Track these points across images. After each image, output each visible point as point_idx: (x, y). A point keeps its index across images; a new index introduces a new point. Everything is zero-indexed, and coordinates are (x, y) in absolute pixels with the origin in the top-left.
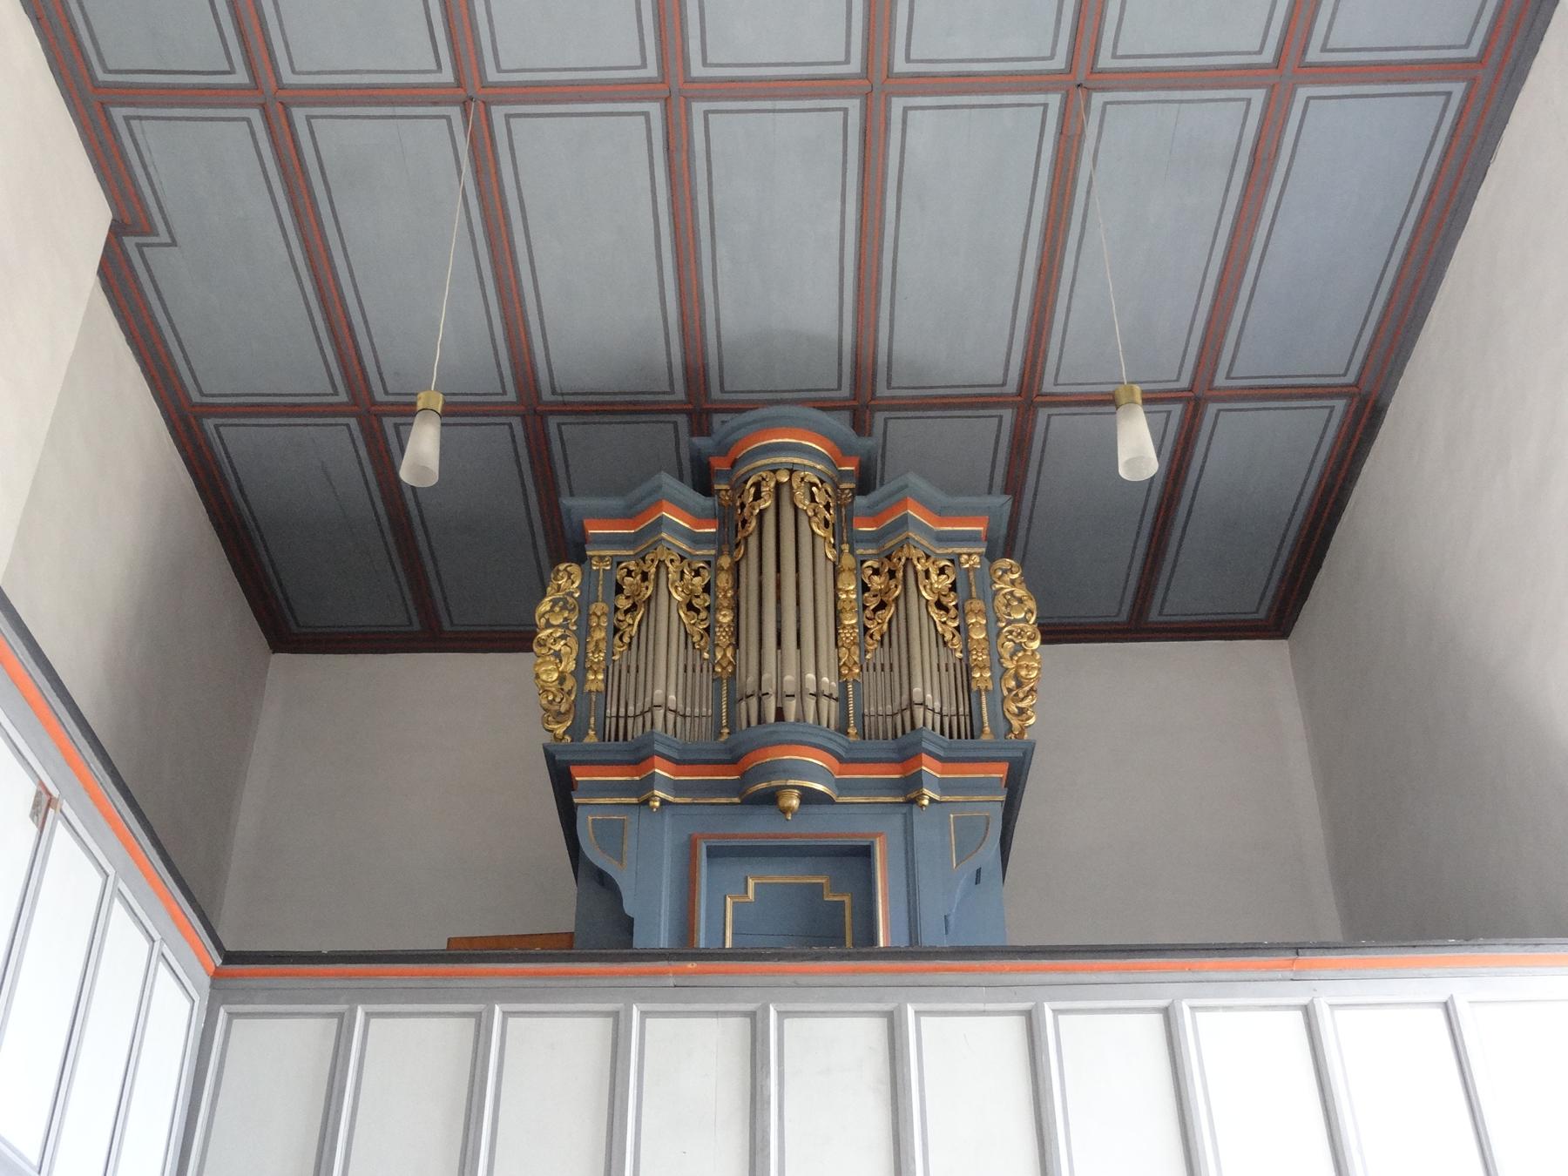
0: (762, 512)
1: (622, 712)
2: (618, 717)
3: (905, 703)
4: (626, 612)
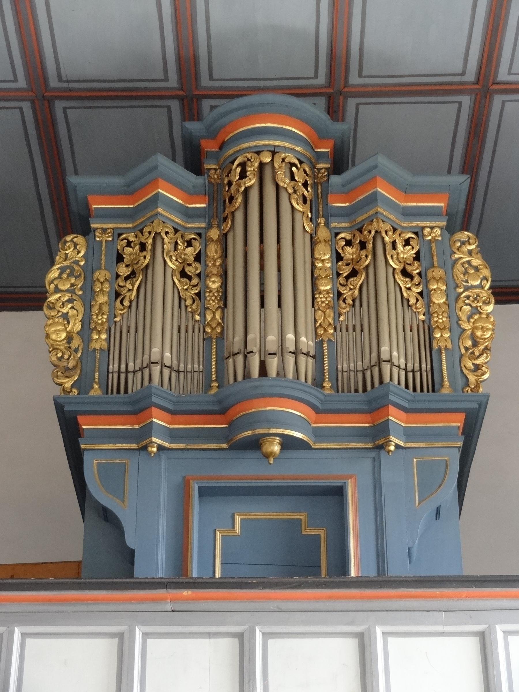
0: (247, 190)
2: (119, 372)
4: (126, 279)
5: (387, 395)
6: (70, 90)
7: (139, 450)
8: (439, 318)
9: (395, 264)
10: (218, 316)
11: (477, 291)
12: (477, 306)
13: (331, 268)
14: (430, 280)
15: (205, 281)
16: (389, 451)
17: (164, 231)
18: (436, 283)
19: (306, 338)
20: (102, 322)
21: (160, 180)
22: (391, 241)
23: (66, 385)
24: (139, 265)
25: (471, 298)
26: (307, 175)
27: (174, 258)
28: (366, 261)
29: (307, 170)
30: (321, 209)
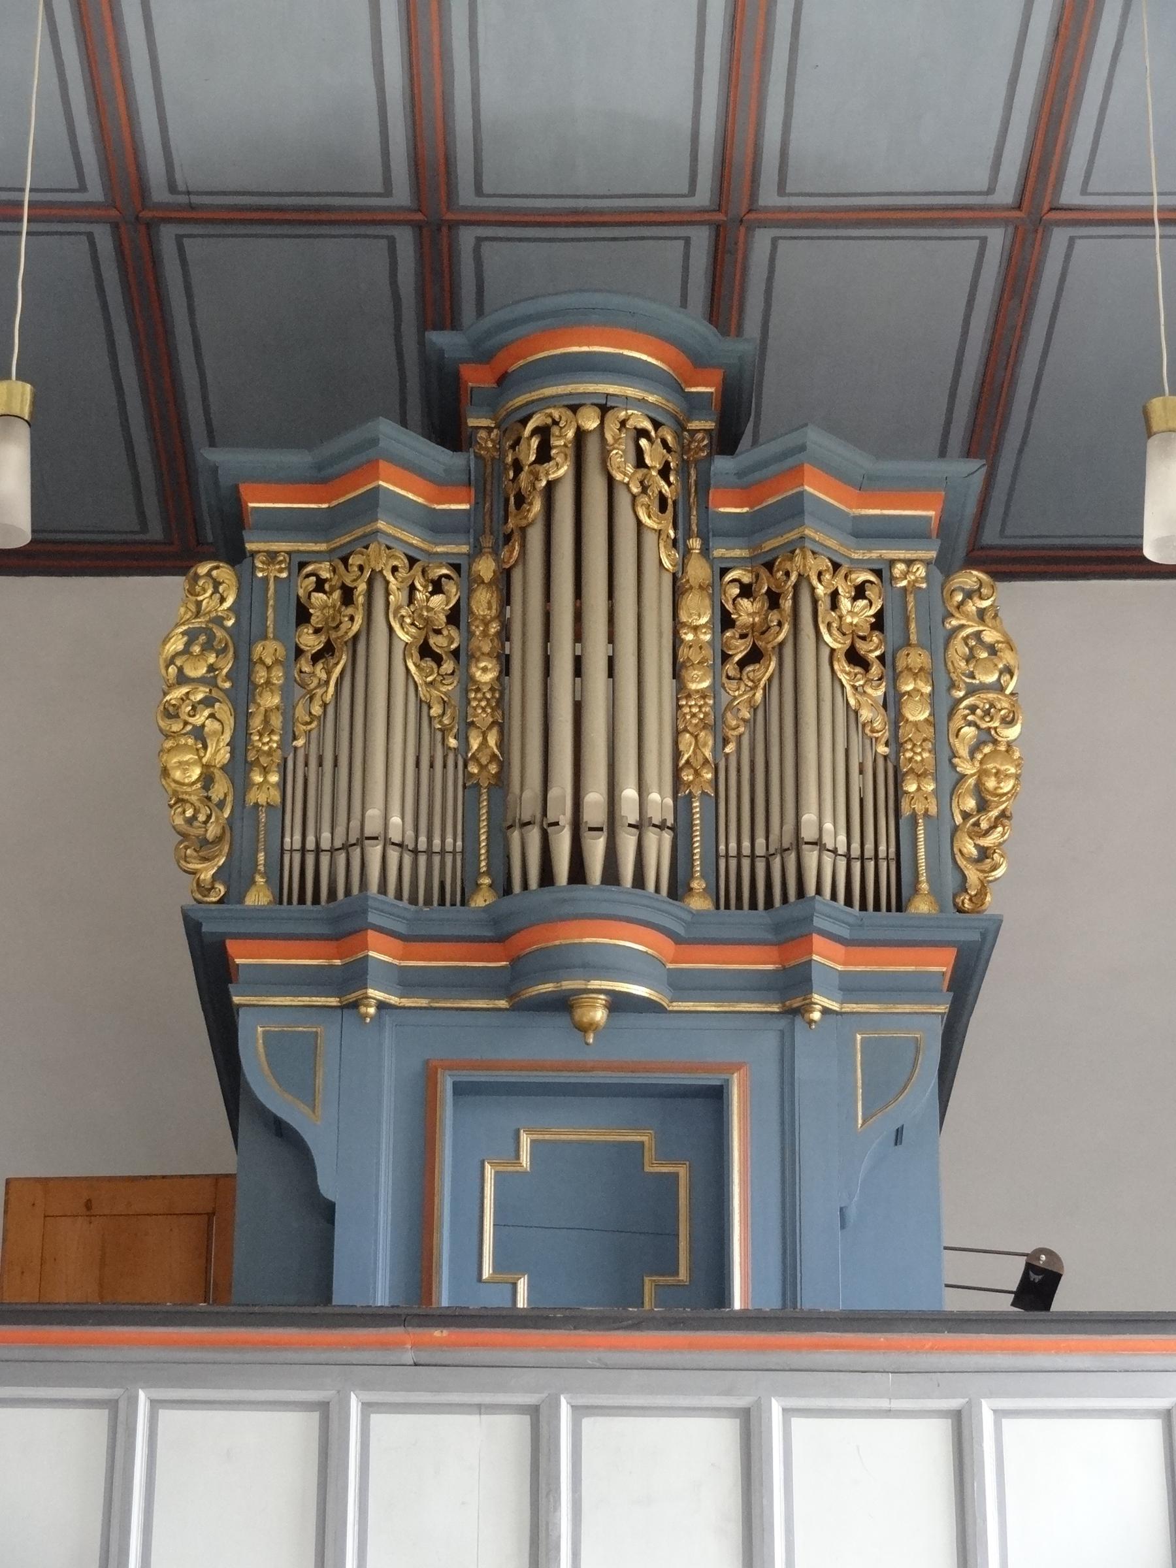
0: (551, 485)
1: (311, 843)
2: (303, 850)
3: (788, 840)
4: (316, 658)
5: (809, 919)
6: (192, 207)
7: (342, 1007)
8: (915, 753)
9: (835, 640)
10: (492, 740)
11: (991, 696)
12: (989, 728)
13: (711, 643)
14: (901, 672)
15: (468, 666)
16: (811, 1022)
17: (389, 567)
18: (911, 680)
19: (660, 793)
20: (271, 748)
21: (382, 464)
22: (829, 591)
23: (202, 877)
24: (340, 633)
25: (979, 712)
26: (669, 450)
27: (408, 620)
28: (778, 633)
29: (669, 439)
30: (694, 519)
